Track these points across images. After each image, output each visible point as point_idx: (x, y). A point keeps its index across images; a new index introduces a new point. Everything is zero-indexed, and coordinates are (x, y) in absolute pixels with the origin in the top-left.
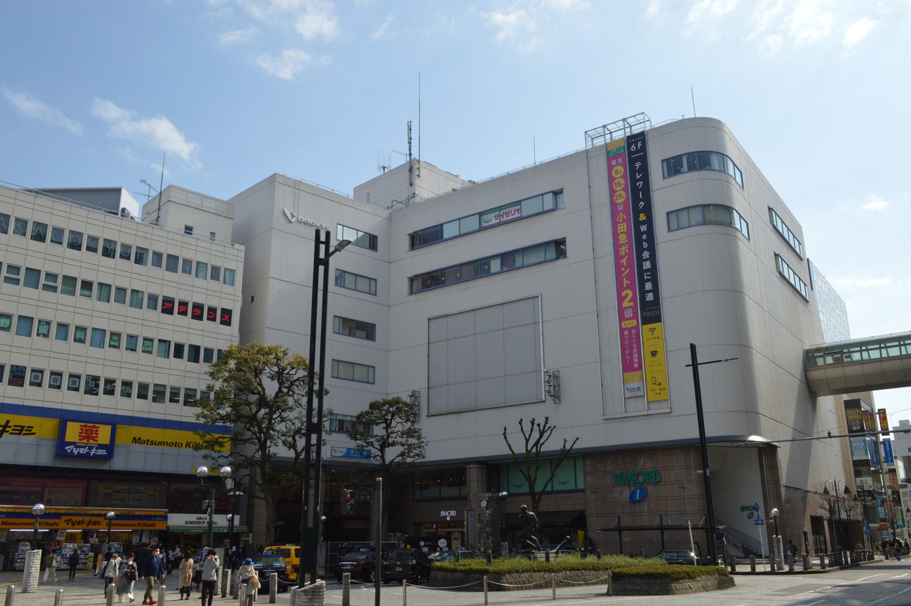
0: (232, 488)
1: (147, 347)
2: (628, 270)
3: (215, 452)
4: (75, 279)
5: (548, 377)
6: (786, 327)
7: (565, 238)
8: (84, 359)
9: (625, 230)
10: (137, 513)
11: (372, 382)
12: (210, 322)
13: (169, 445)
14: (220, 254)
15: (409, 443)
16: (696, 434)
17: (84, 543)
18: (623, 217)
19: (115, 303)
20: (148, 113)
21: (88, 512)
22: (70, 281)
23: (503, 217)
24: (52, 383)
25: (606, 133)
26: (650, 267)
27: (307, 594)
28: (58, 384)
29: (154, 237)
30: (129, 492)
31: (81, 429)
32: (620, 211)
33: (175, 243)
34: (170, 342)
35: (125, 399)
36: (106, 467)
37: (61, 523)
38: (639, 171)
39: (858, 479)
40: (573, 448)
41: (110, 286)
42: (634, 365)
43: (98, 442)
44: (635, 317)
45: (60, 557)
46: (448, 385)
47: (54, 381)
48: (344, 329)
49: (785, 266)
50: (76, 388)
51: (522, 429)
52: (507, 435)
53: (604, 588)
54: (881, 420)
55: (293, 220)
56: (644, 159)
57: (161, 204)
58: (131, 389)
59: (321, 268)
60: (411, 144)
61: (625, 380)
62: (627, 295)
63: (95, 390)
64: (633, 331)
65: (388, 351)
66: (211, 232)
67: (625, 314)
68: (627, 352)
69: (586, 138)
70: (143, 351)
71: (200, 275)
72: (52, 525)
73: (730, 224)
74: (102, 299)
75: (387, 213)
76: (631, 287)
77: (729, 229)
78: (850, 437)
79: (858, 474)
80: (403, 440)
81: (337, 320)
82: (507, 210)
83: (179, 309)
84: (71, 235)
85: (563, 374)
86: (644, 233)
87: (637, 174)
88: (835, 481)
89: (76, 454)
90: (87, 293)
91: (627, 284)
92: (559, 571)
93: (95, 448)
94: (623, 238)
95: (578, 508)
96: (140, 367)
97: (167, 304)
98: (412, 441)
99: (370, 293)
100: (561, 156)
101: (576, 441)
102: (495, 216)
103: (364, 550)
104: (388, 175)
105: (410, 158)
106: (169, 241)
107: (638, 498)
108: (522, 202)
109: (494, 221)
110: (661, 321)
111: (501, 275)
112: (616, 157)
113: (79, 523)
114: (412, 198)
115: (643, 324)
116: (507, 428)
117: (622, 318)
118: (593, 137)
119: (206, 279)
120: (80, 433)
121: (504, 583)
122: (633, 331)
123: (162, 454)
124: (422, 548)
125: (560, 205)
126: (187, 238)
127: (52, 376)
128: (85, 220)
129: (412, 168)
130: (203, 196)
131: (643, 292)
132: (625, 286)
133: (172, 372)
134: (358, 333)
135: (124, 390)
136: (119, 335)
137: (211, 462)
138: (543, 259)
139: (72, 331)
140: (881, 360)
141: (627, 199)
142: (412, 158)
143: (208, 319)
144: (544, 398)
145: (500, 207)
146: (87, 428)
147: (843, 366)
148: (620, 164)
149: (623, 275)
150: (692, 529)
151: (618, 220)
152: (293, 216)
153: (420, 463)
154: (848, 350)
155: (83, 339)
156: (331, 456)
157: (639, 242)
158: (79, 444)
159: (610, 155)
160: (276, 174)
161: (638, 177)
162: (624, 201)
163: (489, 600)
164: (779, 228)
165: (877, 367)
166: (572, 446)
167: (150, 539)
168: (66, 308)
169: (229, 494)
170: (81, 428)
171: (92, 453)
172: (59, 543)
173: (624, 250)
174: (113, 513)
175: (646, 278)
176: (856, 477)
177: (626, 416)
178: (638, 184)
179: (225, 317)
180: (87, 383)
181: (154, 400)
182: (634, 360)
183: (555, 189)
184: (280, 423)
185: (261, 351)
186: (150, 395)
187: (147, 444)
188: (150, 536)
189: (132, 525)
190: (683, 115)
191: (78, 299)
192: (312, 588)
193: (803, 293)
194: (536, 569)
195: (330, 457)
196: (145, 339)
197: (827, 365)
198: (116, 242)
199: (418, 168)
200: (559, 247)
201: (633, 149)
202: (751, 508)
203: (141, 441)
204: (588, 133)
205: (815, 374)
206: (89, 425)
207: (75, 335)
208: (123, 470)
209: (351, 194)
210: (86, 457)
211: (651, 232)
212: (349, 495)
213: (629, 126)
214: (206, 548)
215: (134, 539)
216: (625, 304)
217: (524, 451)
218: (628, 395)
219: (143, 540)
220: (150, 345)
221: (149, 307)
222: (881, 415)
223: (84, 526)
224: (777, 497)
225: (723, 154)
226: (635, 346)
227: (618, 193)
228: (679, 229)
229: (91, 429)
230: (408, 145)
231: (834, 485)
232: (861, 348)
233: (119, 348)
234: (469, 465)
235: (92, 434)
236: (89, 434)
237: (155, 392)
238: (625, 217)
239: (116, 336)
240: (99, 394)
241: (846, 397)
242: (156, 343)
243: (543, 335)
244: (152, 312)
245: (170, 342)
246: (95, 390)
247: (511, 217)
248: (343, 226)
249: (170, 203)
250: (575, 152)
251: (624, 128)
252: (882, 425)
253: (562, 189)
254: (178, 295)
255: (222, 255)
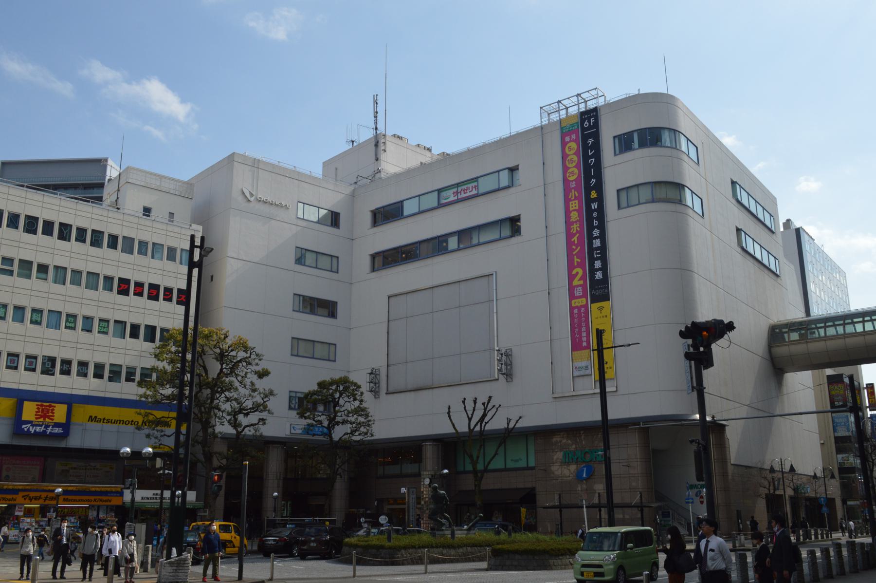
0: (161, 467)
1: (103, 328)
2: (579, 248)
3: (157, 431)
4: (31, 263)
5: (500, 356)
6: (746, 303)
7: (520, 215)
8: (40, 341)
9: (577, 208)
10: (93, 489)
11: (334, 359)
12: (166, 303)
13: (125, 423)
14: (176, 235)
15: (358, 421)
16: (598, 417)
17: (42, 517)
18: (575, 195)
19: (71, 285)
20: (137, 74)
21: (45, 488)
22: (26, 265)
23: (461, 194)
24: (9, 364)
25: (580, 102)
26: (600, 245)
27: (172, 565)
28: (15, 365)
29: (109, 220)
30: (86, 469)
31: (38, 408)
32: (572, 188)
33: (131, 225)
34: (126, 322)
35: (81, 379)
36: (62, 444)
37: (19, 498)
38: (592, 148)
39: (840, 456)
40: (516, 426)
41: (66, 268)
42: (582, 345)
43: (54, 421)
44: (584, 295)
45: (18, 531)
46: (406, 362)
47: (11, 362)
48: (305, 307)
49: (750, 241)
50: (33, 368)
51: (465, 408)
52: (451, 414)
53: (484, 565)
54: (869, 394)
55: (252, 199)
56: (596, 136)
57: (120, 186)
58: (87, 369)
59: (195, 271)
60: (378, 118)
61: (574, 358)
62: (577, 273)
63: (51, 371)
64: (583, 310)
65: (350, 329)
66: (170, 213)
67: (575, 292)
68: (577, 330)
69: (541, 113)
70: (99, 332)
71: (156, 256)
72: (10, 500)
73: (680, 201)
74: (58, 281)
75: (349, 190)
76: (581, 265)
77: (679, 207)
78: (832, 412)
79: (839, 451)
80: (352, 419)
81: (297, 298)
82: (465, 187)
83: (134, 290)
84: (26, 220)
85: (515, 352)
86: (595, 210)
87: (589, 150)
88: (781, 460)
89: (32, 432)
90: (43, 276)
91: (577, 262)
92: (459, 547)
93: (51, 426)
94: (574, 216)
95: (529, 485)
96: (96, 348)
97: (123, 286)
98: (361, 419)
99: (331, 271)
100: (520, 131)
101: (519, 419)
102: (454, 193)
103: (290, 526)
104: (356, 148)
105: (376, 133)
106: (125, 224)
107: (584, 476)
108: (479, 179)
109: (452, 198)
110: (609, 300)
111: (458, 252)
112: (569, 133)
113: (36, 498)
114: (377, 173)
115: (592, 302)
116: (451, 407)
117: (572, 297)
118: (549, 112)
119: (162, 260)
120: (37, 412)
121: (398, 557)
122: (583, 310)
123: (118, 432)
124: (363, 524)
125: (516, 182)
126: (146, 221)
127: (9, 358)
128: (40, 204)
129: (377, 142)
130: (162, 177)
131: (593, 271)
132: (576, 264)
133: (127, 352)
134: (320, 310)
135: (80, 370)
136: (75, 317)
137: (153, 440)
138: (497, 236)
139: (28, 314)
140: (837, 337)
141: (580, 176)
142: (378, 132)
143: (164, 299)
144: (496, 376)
145: (458, 184)
146: (44, 407)
147: (807, 343)
148: (573, 141)
149: (574, 253)
150: (586, 507)
151: (570, 197)
152: (252, 195)
153: (369, 441)
154: (871, 318)
155: (39, 321)
156: (291, 433)
157: (590, 219)
158: (36, 423)
159: (564, 131)
160: (234, 153)
161: (590, 154)
162: (577, 178)
163: (358, 573)
164: (745, 202)
165: (839, 343)
166: (515, 425)
167: (107, 514)
168: (22, 291)
169: (159, 473)
170: (37, 407)
171: (48, 432)
172: (17, 517)
173: (575, 227)
174: (61, 490)
175: (595, 256)
176: (837, 454)
177: (574, 395)
178: (590, 160)
179: (181, 297)
180: (43, 364)
181: (111, 379)
182: (583, 338)
183: (511, 165)
184: (225, 403)
185: (201, 334)
186: (106, 374)
187: (103, 422)
188: (107, 510)
189: (88, 500)
190: (639, 90)
191: (35, 282)
192: (177, 560)
193: (773, 267)
194: (434, 545)
195: (289, 434)
196: (101, 320)
197: (792, 341)
198: (71, 226)
199: (384, 143)
200: (513, 224)
201: (586, 125)
202: (699, 486)
203: (97, 420)
204: (543, 108)
205: (781, 351)
206: (45, 404)
207: (31, 317)
208: (79, 447)
209: (317, 171)
210: (43, 435)
211: (601, 210)
212: (216, 478)
213: (583, 101)
214: (128, 523)
215: (90, 514)
216: (576, 282)
217: (467, 430)
218: (576, 373)
219: (100, 516)
220: (106, 326)
221: (104, 289)
222: (869, 390)
223: (41, 501)
224: (723, 476)
225: (675, 130)
226: (583, 324)
227: (570, 170)
228: (628, 206)
229: (46, 409)
230: (373, 119)
231: (780, 463)
232: (825, 324)
233: (75, 329)
234: (425, 442)
235: (48, 413)
236: (46, 413)
237: (111, 372)
238: (577, 195)
239: (72, 317)
240: (55, 375)
241: (829, 372)
242: (112, 323)
243: (497, 312)
244: (107, 293)
245: (126, 322)
246: (51, 371)
247: (469, 194)
248: (304, 204)
249: (129, 185)
250: (482, 144)
251: (578, 104)
252: (870, 399)
253: (518, 166)
254: (134, 277)
255: (179, 236)
